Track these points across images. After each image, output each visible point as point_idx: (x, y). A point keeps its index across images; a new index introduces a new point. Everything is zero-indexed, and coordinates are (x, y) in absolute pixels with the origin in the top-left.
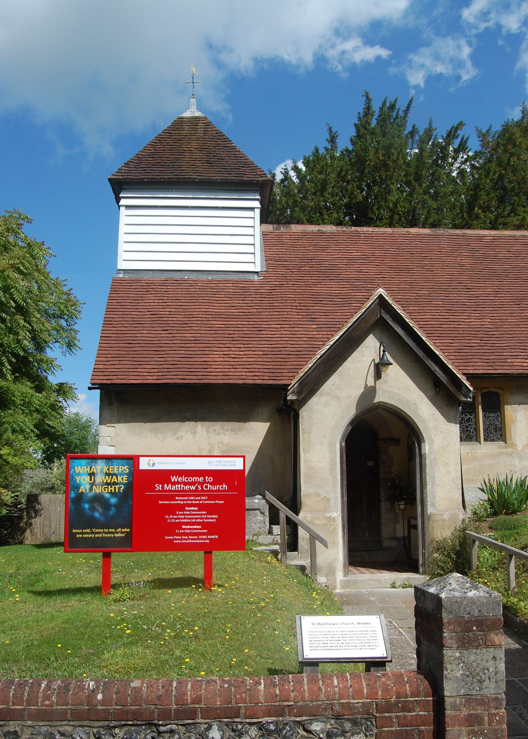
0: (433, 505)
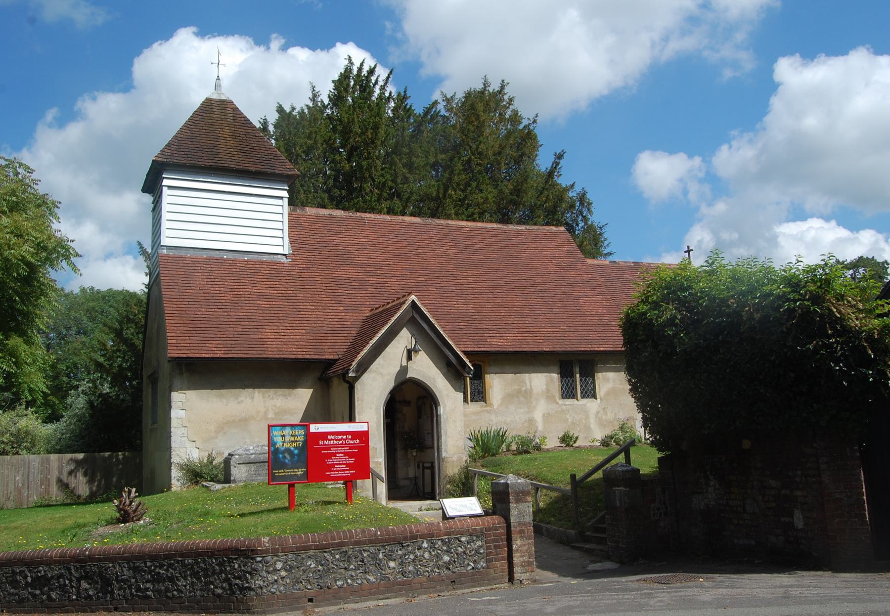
0: (446, 451)
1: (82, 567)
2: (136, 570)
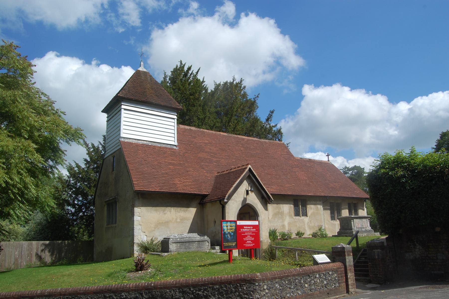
1: (149, 292)
2: (183, 292)
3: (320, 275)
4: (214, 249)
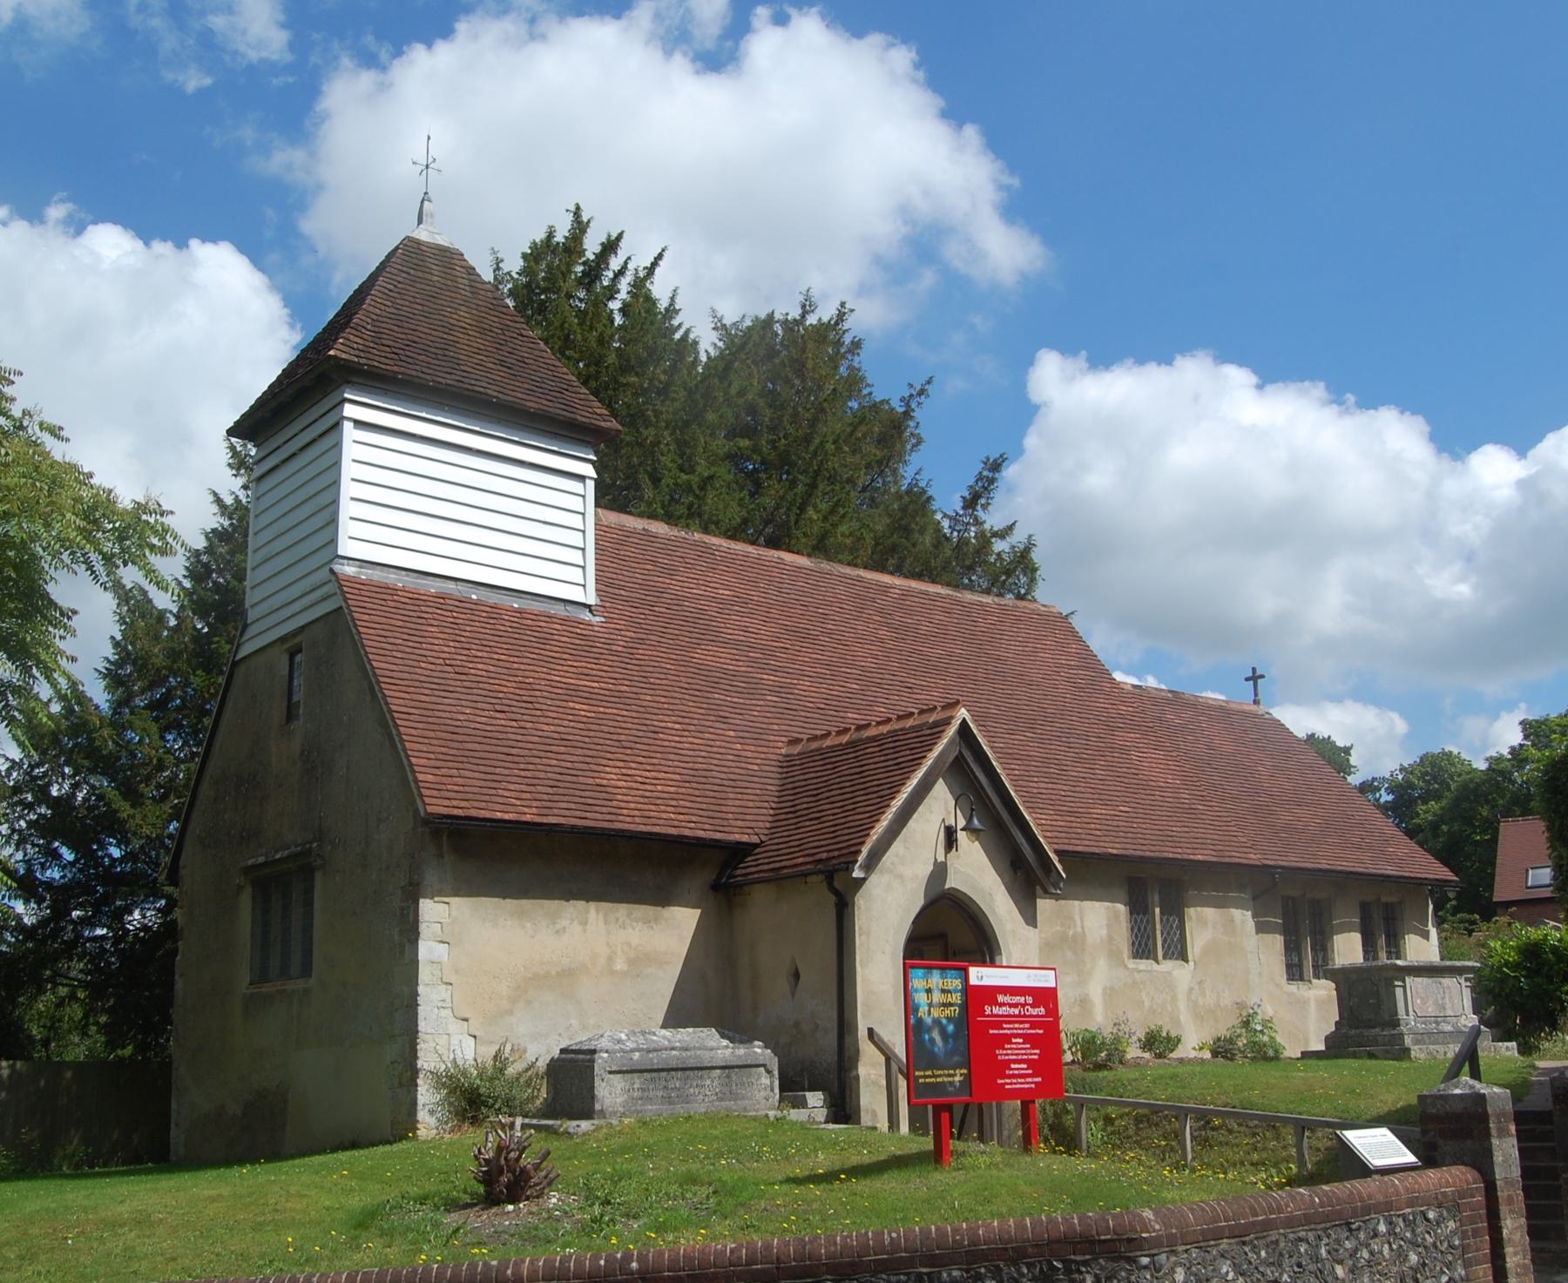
3: (1390, 1223)
4: (801, 1104)
